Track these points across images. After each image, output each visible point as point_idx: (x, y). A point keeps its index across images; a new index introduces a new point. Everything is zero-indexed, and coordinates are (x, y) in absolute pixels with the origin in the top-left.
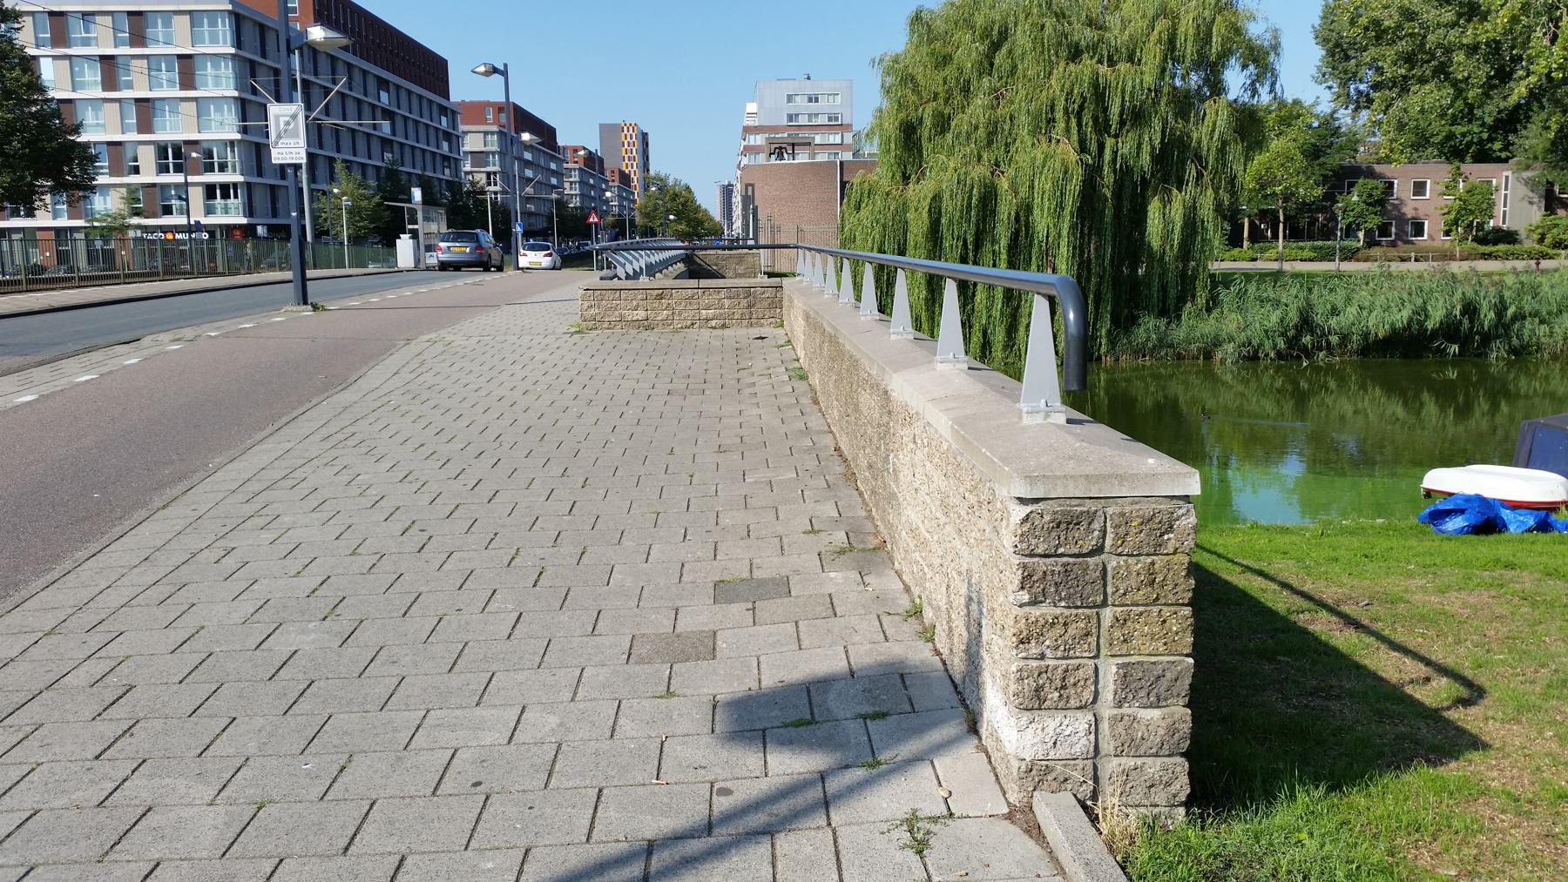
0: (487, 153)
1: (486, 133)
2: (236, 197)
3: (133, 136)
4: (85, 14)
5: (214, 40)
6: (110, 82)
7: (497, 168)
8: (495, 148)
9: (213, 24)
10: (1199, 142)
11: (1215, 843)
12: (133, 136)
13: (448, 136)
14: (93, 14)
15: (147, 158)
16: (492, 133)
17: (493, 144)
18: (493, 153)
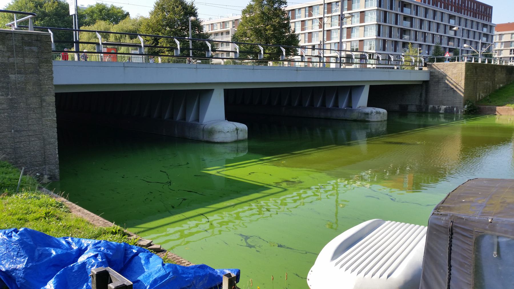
5: (371, 5)
13: (486, 35)
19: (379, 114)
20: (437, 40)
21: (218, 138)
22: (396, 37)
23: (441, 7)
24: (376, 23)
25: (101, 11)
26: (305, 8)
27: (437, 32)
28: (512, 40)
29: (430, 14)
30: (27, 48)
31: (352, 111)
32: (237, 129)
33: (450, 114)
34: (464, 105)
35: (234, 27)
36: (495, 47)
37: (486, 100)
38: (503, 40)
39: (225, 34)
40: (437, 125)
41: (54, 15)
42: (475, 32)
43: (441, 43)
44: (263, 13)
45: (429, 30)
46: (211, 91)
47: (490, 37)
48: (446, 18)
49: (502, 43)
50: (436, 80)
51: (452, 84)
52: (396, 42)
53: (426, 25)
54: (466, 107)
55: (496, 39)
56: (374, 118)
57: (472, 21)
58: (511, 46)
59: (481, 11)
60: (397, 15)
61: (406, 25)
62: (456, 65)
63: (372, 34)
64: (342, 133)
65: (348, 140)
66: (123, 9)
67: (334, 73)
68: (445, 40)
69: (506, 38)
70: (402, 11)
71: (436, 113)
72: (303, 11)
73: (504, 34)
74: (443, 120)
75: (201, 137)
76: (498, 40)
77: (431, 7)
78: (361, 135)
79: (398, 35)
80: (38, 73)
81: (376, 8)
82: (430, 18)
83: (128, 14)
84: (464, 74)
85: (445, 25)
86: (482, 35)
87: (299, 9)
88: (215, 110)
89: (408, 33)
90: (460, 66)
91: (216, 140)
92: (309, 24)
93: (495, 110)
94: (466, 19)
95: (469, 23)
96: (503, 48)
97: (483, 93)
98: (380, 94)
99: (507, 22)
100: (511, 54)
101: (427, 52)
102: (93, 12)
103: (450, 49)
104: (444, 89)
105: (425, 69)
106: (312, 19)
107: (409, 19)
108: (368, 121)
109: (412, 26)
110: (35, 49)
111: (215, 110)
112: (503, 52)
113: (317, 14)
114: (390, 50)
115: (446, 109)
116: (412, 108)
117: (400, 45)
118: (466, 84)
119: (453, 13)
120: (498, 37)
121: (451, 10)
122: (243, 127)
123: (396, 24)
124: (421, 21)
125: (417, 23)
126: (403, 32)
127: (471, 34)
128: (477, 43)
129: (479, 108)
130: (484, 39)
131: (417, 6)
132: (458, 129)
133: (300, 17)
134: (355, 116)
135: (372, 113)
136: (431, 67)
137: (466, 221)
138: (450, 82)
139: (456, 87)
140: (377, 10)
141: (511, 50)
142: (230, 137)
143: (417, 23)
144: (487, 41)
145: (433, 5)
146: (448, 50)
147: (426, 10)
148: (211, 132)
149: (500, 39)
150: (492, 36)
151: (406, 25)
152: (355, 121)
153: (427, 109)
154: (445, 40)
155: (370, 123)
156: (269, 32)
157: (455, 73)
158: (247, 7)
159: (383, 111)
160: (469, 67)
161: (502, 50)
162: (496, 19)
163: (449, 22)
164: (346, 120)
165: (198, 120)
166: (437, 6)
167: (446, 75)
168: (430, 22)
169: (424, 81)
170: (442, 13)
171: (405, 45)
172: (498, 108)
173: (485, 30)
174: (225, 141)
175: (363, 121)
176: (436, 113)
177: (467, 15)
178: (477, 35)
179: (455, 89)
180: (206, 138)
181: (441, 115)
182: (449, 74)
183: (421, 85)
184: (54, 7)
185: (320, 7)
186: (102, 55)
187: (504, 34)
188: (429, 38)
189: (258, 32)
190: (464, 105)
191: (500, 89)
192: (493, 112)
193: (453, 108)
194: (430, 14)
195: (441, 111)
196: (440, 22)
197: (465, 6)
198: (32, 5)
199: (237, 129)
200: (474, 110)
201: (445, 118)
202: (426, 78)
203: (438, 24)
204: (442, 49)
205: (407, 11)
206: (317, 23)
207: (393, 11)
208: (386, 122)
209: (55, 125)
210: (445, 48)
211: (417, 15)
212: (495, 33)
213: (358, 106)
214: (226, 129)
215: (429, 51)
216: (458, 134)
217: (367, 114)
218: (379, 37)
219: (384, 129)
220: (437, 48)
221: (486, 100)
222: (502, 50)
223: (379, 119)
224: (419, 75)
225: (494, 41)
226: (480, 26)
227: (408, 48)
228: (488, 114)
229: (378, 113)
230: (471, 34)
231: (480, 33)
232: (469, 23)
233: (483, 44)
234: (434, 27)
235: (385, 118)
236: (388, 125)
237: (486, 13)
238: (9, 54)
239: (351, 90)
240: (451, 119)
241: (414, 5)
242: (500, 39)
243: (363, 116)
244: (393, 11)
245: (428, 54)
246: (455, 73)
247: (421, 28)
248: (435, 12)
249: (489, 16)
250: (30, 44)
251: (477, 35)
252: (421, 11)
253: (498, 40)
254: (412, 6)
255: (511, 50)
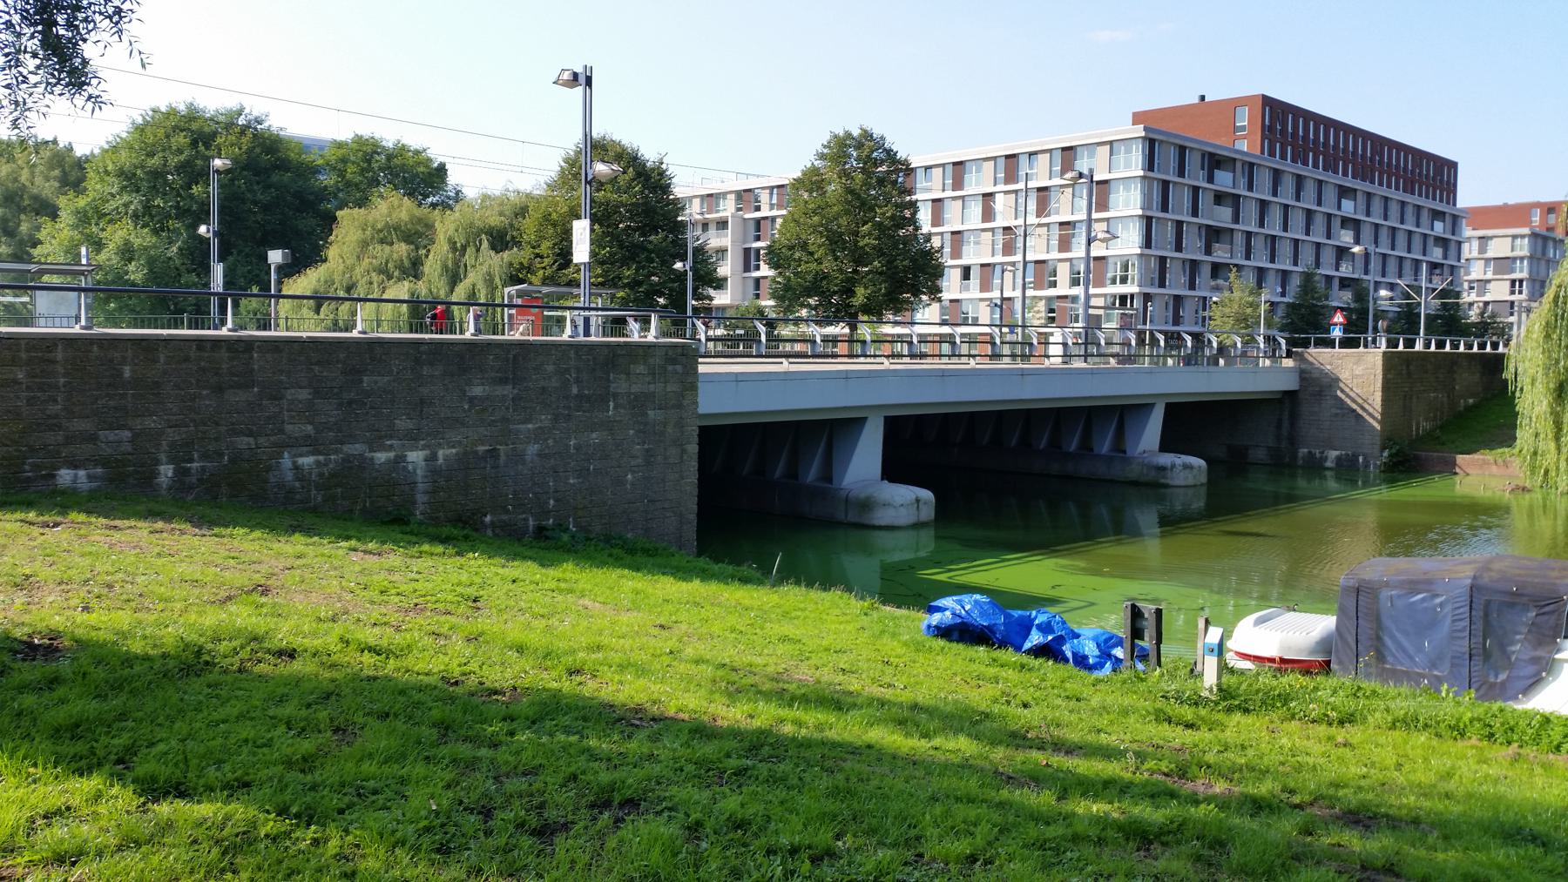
0: (1514, 259)
1: (1514, 237)
2: (1520, 292)
3: (1055, 255)
4: (1031, 154)
5: (1128, 166)
6: (1042, 209)
7: (1525, 275)
8: (1525, 252)
9: (1128, 151)
10: (1399, 306)
11: (175, 697)
12: (1055, 255)
13: (1443, 242)
14: (1036, 153)
15: (1063, 274)
16: (1523, 237)
17: (1523, 248)
18: (1522, 259)
19: (1188, 468)
20: (1307, 256)
21: (882, 517)
22: (1193, 249)
23: (1316, 166)
24: (1140, 212)
25: (368, 158)
26: (943, 165)
27: (1308, 234)
28: (1515, 254)
29: (1288, 185)
30: (670, 368)
31: (1127, 461)
32: (918, 501)
33: (1349, 471)
34: (1383, 449)
35: (739, 209)
36: (1468, 273)
37: (1431, 439)
38: (1490, 254)
39: (712, 227)
40: (1323, 497)
41: (243, 169)
42: (1410, 232)
43: (1318, 265)
44: (850, 191)
45: (1285, 230)
46: (863, 420)
47: (1453, 246)
48: (1330, 194)
49: (1487, 260)
50: (1315, 389)
51: (1354, 401)
52: (1194, 264)
53: (1275, 215)
54: (1386, 454)
55: (1470, 250)
56: (1180, 478)
57: (1403, 204)
58: (1513, 271)
59: (1427, 175)
60: (1196, 189)
61: (1222, 216)
62: (1361, 355)
63: (1129, 243)
64: (1103, 511)
65: (1122, 529)
66: (431, 153)
67: (1057, 364)
68: (1328, 256)
69: (1499, 248)
70: (1211, 179)
71: (1315, 467)
72: (937, 172)
73: (1491, 238)
74: (1332, 484)
75: (841, 516)
76: (1475, 254)
77: (1289, 167)
78: (1147, 518)
79: (1200, 244)
80: (680, 406)
81: (1141, 173)
82: (1286, 196)
83: (441, 170)
84: (1380, 377)
85: (1329, 216)
86: (1431, 242)
87: (927, 168)
88: (864, 462)
89: (1227, 237)
90: (1370, 358)
91: (877, 522)
92: (952, 211)
93: (1454, 464)
94: (1386, 199)
95: (1394, 209)
96: (1489, 275)
97: (1426, 420)
98: (1190, 422)
99: (1499, 202)
100: (1513, 293)
101: (1279, 290)
102: (344, 160)
103: (1342, 279)
104: (1334, 411)
105: (1288, 363)
106: (963, 197)
107: (1229, 201)
108: (1166, 486)
109: (1236, 220)
110: (679, 368)
111: (864, 462)
112: (1490, 286)
113: (977, 183)
114: (1177, 284)
115: (1339, 459)
116: (1259, 454)
117: (1206, 271)
118: (1386, 401)
119: (1349, 182)
120: (1475, 244)
121: (1345, 174)
122: (927, 495)
123: (1195, 213)
124: (1263, 205)
125: (1250, 211)
126: (1213, 235)
127: (1401, 239)
128: (1417, 263)
129: (1417, 458)
130: (1436, 254)
131: (1251, 165)
132: (1374, 501)
133: (929, 190)
134: (1133, 472)
135: (1173, 466)
136: (1301, 358)
137: (1369, 582)
138: (1348, 396)
139: (1363, 408)
140: (1144, 177)
141: (1513, 282)
142: (904, 517)
143: (1250, 211)
144: (1445, 257)
145: (1294, 160)
146: (1336, 283)
147: (1277, 175)
148: (867, 505)
149: (1482, 250)
150: (1459, 243)
151: (1222, 216)
152: (1135, 484)
153: (1294, 456)
154: (1328, 256)
155: (1169, 491)
156: (867, 240)
157: (1359, 373)
158: (804, 173)
159: (1198, 462)
160: (1391, 363)
161: (1489, 281)
162: (1468, 195)
163: (1339, 208)
164: (1111, 481)
165: (829, 480)
166: (1305, 163)
167: (1338, 380)
168: (1286, 207)
169: (1285, 392)
170: (1320, 182)
171: (1217, 270)
172: (1460, 458)
173: (1439, 226)
174: (897, 523)
175: (1153, 486)
176: (1315, 467)
177: (1389, 186)
178: (1417, 242)
179: (1360, 412)
180: (852, 517)
181: (1328, 473)
182: (1344, 375)
183: (1280, 401)
184: (245, 148)
185: (986, 164)
186: (513, 311)
187: (1491, 238)
188: (1285, 249)
189: (835, 241)
190: (1383, 449)
191: (1469, 409)
192: (1449, 468)
193: (1356, 457)
194: (1288, 185)
195: (1329, 464)
196: (1315, 208)
197: (1381, 162)
198: (182, 140)
199: (918, 501)
200: (1409, 457)
201: (1338, 479)
202: (1291, 384)
203: (1309, 213)
204: (1321, 285)
205: (1224, 180)
206: (976, 209)
207: (1186, 181)
208: (1203, 491)
209: (696, 492)
210: (1329, 278)
211: (1250, 188)
212: (1468, 232)
213: (1141, 448)
214: (898, 500)
215: (1283, 287)
216: (1370, 517)
217: (1162, 469)
218: (1147, 251)
219: (1202, 504)
220: (1308, 277)
221: (1431, 439)
222: (1489, 281)
223: (1191, 482)
224: (1267, 371)
225: (1466, 253)
226: (1425, 216)
227: (1226, 279)
228: (1439, 472)
229: (1187, 467)
230: (1401, 239)
231: (1425, 236)
232: (1394, 209)
233: (1434, 266)
234: (1297, 219)
235: (1203, 479)
236: (1209, 495)
237: (1441, 181)
238: (649, 379)
239: (1125, 413)
240: (1352, 483)
241: (1244, 163)
242: (1482, 250)
243: (1153, 473)
244: (1186, 181)
245: (1283, 294)
246: (1359, 373)
247: (1262, 225)
248: (1300, 180)
249: (1450, 190)
250: (673, 361)
251: (1417, 242)
252: (1264, 180)
253: (1475, 254)
254: (1239, 165)
255: (1513, 282)
